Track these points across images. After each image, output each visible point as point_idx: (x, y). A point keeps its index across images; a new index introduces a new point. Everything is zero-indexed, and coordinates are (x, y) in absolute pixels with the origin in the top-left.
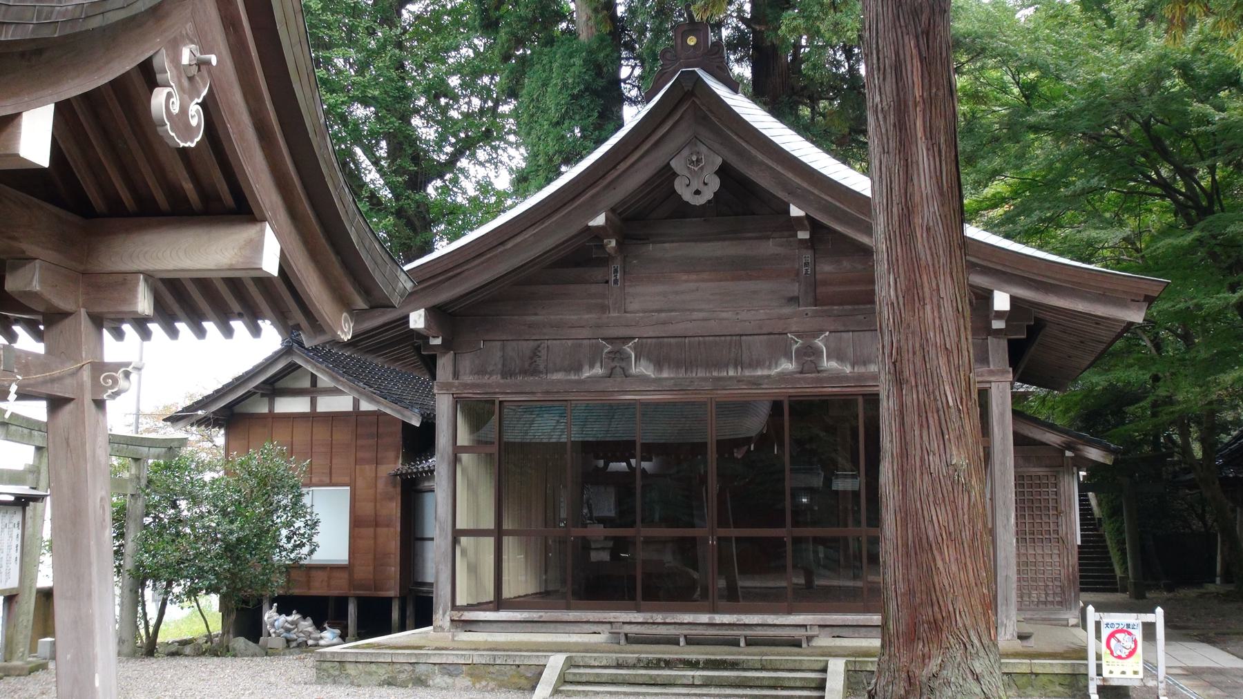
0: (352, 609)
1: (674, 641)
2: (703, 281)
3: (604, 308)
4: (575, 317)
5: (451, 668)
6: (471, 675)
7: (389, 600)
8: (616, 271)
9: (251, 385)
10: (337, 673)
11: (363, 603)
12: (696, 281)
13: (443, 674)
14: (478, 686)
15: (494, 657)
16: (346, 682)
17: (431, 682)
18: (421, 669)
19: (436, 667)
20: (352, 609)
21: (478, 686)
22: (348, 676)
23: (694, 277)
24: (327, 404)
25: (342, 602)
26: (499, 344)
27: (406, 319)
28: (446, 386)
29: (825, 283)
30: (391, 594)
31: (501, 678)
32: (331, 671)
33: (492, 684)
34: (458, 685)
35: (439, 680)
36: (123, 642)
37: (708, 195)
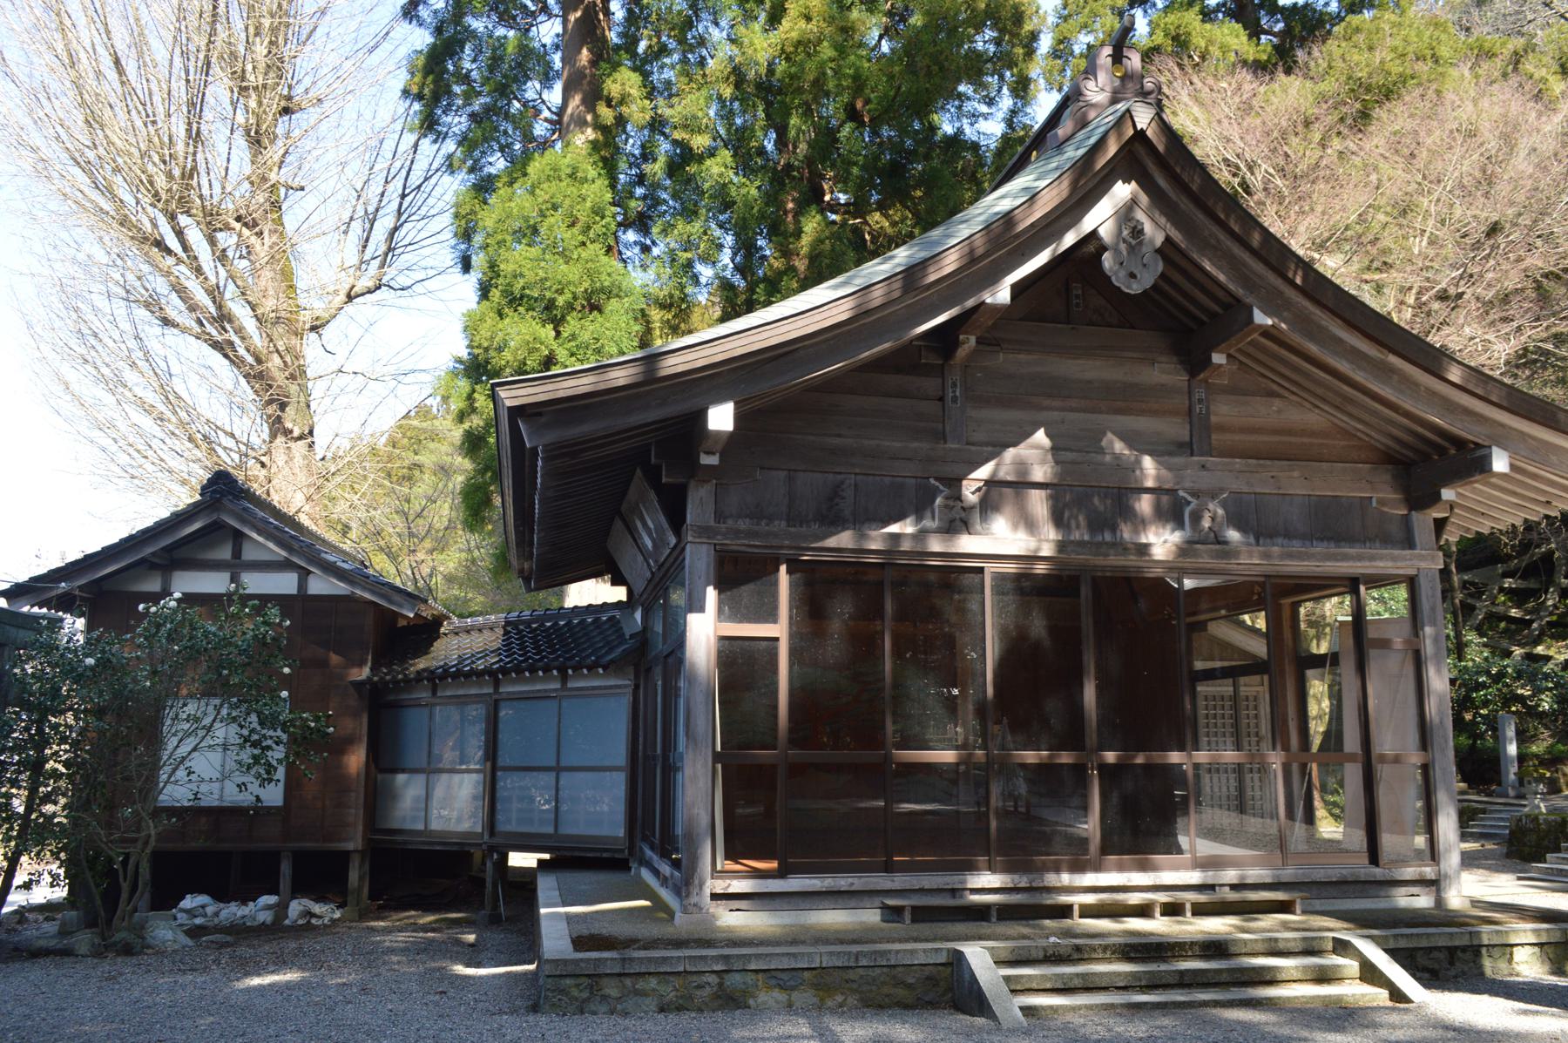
0: (286, 868)
1: (1144, 911)
2: (1072, 410)
3: (942, 436)
4: (898, 445)
5: (784, 976)
6: (816, 986)
7: (345, 856)
8: (954, 385)
9: (148, 550)
10: (585, 995)
11: (299, 858)
12: (1062, 409)
13: (770, 988)
14: (830, 1003)
15: (857, 956)
16: (604, 1008)
17: (751, 1002)
18: (735, 980)
19: (760, 976)
20: (286, 868)
21: (830, 1003)
22: (605, 998)
23: (1057, 403)
24: (256, 583)
25: (273, 858)
26: (783, 474)
27: (702, 415)
28: (704, 531)
29: (1222, 428)
30: (350, 846)
31: (865, 988)
32: (575, 992)
33: (852, 1001)
34: (798, 1004)
35: (768, 997)
36: (790, 1006)
37: (1135, 288)
